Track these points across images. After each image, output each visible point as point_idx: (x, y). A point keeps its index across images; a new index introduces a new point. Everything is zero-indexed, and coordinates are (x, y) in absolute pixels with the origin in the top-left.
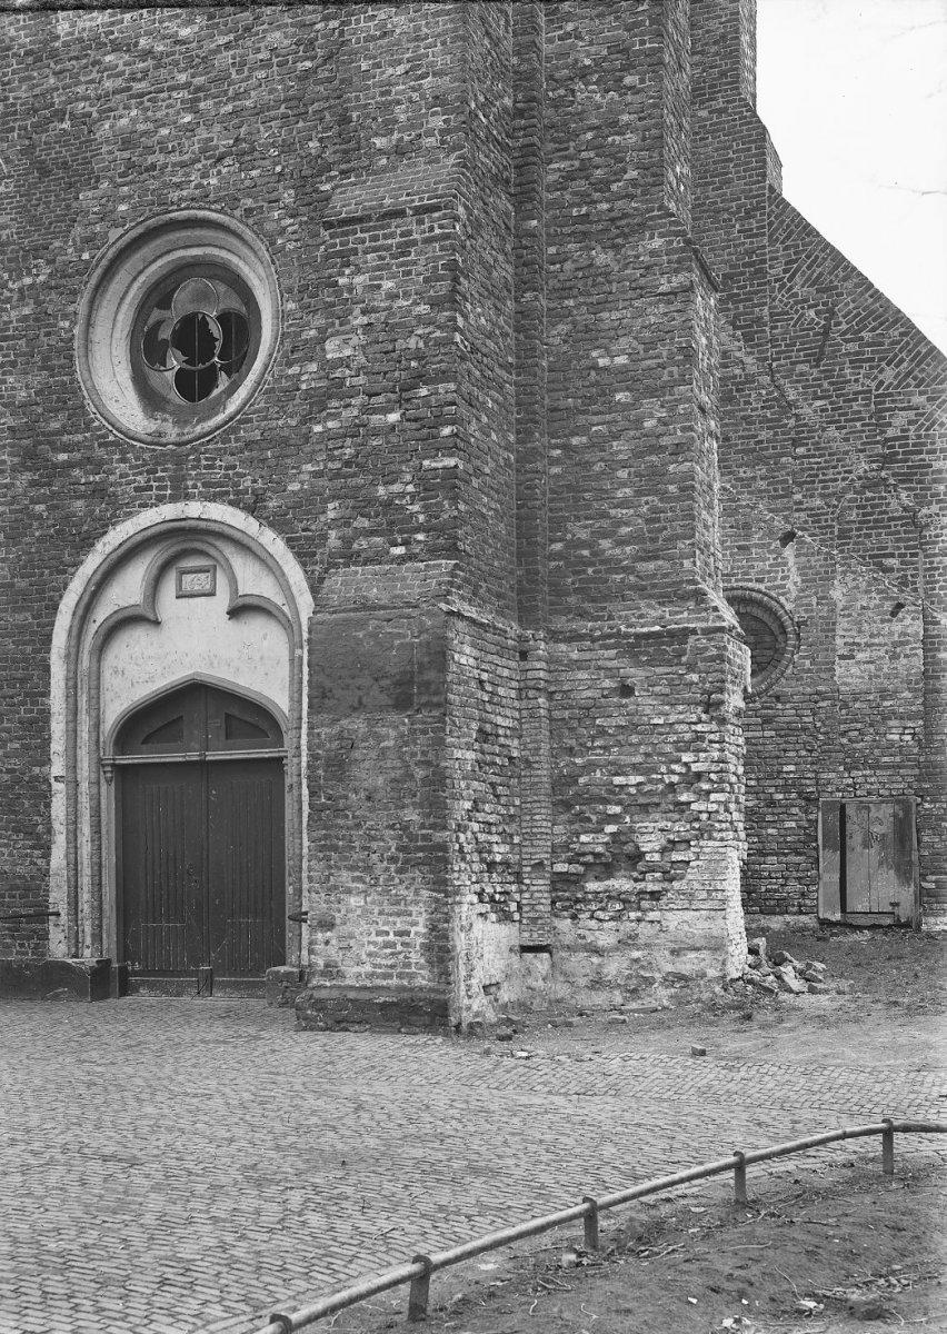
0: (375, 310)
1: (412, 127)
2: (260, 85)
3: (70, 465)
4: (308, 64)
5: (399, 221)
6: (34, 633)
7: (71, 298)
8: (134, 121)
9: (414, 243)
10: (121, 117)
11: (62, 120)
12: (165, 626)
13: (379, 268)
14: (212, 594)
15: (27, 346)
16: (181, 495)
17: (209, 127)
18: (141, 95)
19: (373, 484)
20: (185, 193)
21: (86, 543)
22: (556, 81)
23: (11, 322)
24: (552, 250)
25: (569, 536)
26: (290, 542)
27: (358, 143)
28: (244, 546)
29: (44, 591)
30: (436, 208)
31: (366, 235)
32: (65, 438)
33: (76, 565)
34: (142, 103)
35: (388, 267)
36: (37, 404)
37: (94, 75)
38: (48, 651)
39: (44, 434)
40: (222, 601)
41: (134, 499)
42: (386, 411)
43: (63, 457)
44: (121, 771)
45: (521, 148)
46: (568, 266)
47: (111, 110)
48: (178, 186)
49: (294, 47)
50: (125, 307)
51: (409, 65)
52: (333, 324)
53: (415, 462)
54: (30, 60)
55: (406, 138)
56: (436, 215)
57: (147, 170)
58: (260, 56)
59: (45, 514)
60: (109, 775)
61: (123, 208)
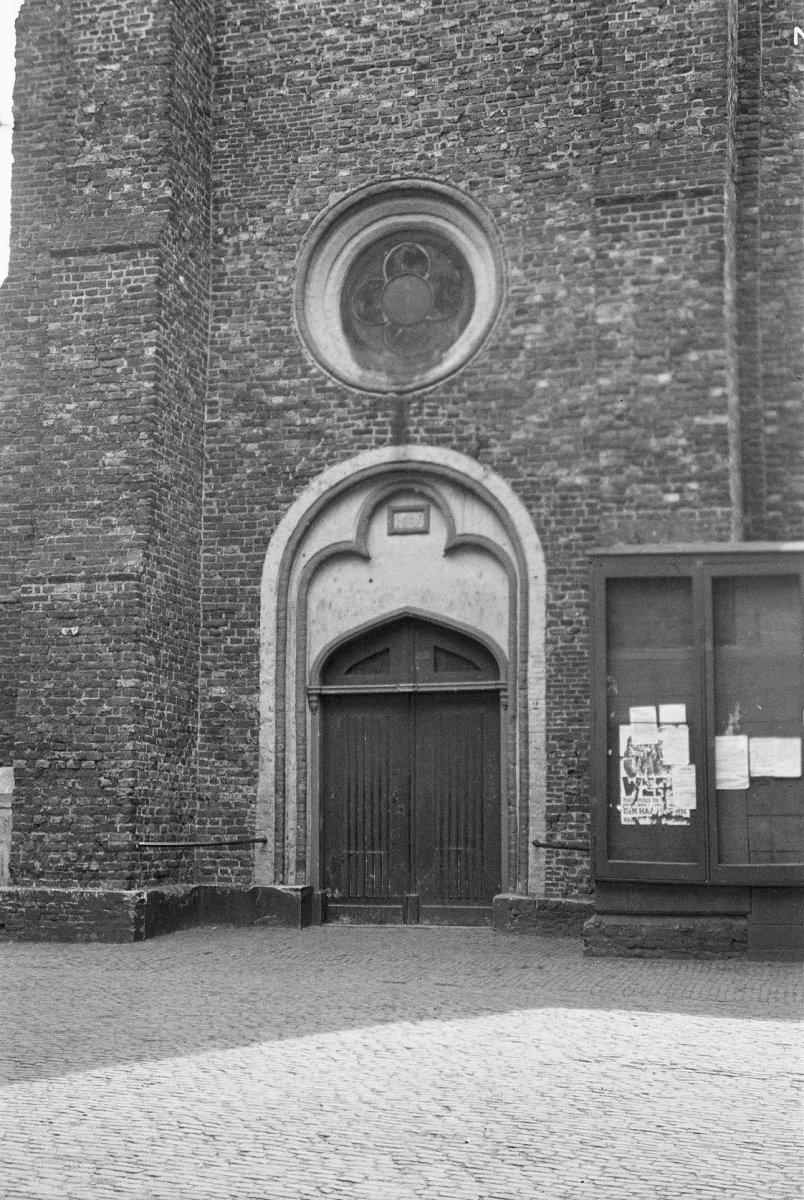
0: (645, 282)
1: (675, 116)
2: (486, 67)
3: (286, 408)
4: (535, 51)
5: (670, 202)
6: (243, 566)
7: (288, 255)
8: (356, 92)
9: (684, 224)
10: (342, 87)
11: (280, 86)
12: (373, 559)
13: (648, 245)
14: (424, 532)
15: (242, 297)
16: (401, 438)
17: (433, 102)
18: (365, 68)
19: (645, 437)
20: (408, 163)
21: (302, 480)
22: (772, 82)
23: (226, 274)
24: (766, 235)
25: (785, 490)
26: (515, 487)
27: (621, 126)
28: (467, 489)
29: (254, 526)
30: (707, 192)
31: (637, 214)
32: (281, 382)
33: (291, 500)
34: (364, 75)
35: (658, 244)
36: (252, 350)
37: (314, 46)
38: (258, 583)
39: (258, 378)
40: (438, 538)
41: (352, 442)
42: (656, 372)
43: (278, 400)
44: (326, 702)
45: (744, 141)
46: (780, 250)
47: (330, 79)
48: (401, 156)
49: (520, 34)
50: (337, 267)
51: (672, 60)
52: (603, 293)
53: (686, 418)
54: (247, 29)
55: (669, 126)
56: (706, 199)
57: (369, 139)
58: (487, 41)
59: (257, 453)
60: (314, 705)
61: (344, 173)
